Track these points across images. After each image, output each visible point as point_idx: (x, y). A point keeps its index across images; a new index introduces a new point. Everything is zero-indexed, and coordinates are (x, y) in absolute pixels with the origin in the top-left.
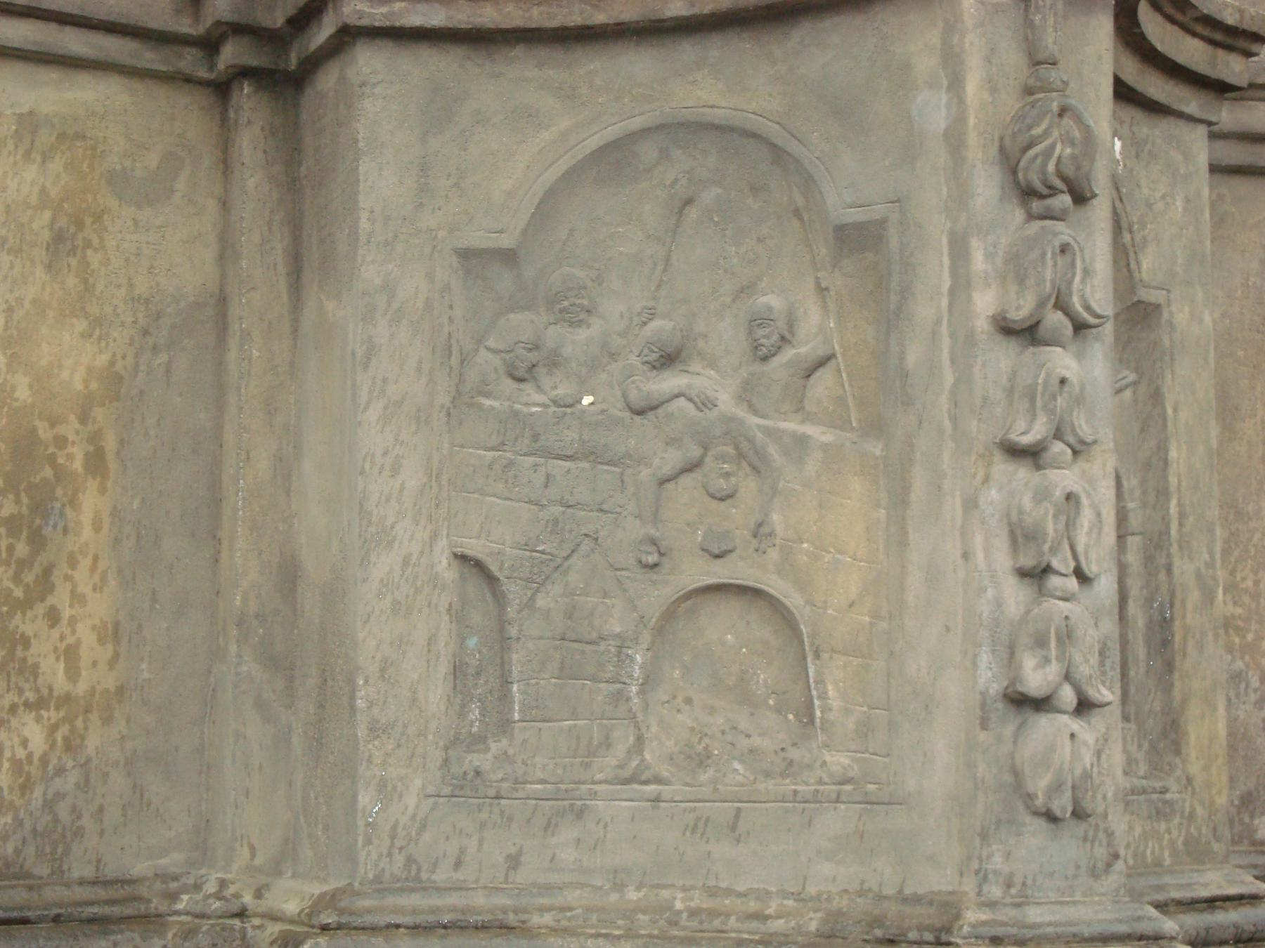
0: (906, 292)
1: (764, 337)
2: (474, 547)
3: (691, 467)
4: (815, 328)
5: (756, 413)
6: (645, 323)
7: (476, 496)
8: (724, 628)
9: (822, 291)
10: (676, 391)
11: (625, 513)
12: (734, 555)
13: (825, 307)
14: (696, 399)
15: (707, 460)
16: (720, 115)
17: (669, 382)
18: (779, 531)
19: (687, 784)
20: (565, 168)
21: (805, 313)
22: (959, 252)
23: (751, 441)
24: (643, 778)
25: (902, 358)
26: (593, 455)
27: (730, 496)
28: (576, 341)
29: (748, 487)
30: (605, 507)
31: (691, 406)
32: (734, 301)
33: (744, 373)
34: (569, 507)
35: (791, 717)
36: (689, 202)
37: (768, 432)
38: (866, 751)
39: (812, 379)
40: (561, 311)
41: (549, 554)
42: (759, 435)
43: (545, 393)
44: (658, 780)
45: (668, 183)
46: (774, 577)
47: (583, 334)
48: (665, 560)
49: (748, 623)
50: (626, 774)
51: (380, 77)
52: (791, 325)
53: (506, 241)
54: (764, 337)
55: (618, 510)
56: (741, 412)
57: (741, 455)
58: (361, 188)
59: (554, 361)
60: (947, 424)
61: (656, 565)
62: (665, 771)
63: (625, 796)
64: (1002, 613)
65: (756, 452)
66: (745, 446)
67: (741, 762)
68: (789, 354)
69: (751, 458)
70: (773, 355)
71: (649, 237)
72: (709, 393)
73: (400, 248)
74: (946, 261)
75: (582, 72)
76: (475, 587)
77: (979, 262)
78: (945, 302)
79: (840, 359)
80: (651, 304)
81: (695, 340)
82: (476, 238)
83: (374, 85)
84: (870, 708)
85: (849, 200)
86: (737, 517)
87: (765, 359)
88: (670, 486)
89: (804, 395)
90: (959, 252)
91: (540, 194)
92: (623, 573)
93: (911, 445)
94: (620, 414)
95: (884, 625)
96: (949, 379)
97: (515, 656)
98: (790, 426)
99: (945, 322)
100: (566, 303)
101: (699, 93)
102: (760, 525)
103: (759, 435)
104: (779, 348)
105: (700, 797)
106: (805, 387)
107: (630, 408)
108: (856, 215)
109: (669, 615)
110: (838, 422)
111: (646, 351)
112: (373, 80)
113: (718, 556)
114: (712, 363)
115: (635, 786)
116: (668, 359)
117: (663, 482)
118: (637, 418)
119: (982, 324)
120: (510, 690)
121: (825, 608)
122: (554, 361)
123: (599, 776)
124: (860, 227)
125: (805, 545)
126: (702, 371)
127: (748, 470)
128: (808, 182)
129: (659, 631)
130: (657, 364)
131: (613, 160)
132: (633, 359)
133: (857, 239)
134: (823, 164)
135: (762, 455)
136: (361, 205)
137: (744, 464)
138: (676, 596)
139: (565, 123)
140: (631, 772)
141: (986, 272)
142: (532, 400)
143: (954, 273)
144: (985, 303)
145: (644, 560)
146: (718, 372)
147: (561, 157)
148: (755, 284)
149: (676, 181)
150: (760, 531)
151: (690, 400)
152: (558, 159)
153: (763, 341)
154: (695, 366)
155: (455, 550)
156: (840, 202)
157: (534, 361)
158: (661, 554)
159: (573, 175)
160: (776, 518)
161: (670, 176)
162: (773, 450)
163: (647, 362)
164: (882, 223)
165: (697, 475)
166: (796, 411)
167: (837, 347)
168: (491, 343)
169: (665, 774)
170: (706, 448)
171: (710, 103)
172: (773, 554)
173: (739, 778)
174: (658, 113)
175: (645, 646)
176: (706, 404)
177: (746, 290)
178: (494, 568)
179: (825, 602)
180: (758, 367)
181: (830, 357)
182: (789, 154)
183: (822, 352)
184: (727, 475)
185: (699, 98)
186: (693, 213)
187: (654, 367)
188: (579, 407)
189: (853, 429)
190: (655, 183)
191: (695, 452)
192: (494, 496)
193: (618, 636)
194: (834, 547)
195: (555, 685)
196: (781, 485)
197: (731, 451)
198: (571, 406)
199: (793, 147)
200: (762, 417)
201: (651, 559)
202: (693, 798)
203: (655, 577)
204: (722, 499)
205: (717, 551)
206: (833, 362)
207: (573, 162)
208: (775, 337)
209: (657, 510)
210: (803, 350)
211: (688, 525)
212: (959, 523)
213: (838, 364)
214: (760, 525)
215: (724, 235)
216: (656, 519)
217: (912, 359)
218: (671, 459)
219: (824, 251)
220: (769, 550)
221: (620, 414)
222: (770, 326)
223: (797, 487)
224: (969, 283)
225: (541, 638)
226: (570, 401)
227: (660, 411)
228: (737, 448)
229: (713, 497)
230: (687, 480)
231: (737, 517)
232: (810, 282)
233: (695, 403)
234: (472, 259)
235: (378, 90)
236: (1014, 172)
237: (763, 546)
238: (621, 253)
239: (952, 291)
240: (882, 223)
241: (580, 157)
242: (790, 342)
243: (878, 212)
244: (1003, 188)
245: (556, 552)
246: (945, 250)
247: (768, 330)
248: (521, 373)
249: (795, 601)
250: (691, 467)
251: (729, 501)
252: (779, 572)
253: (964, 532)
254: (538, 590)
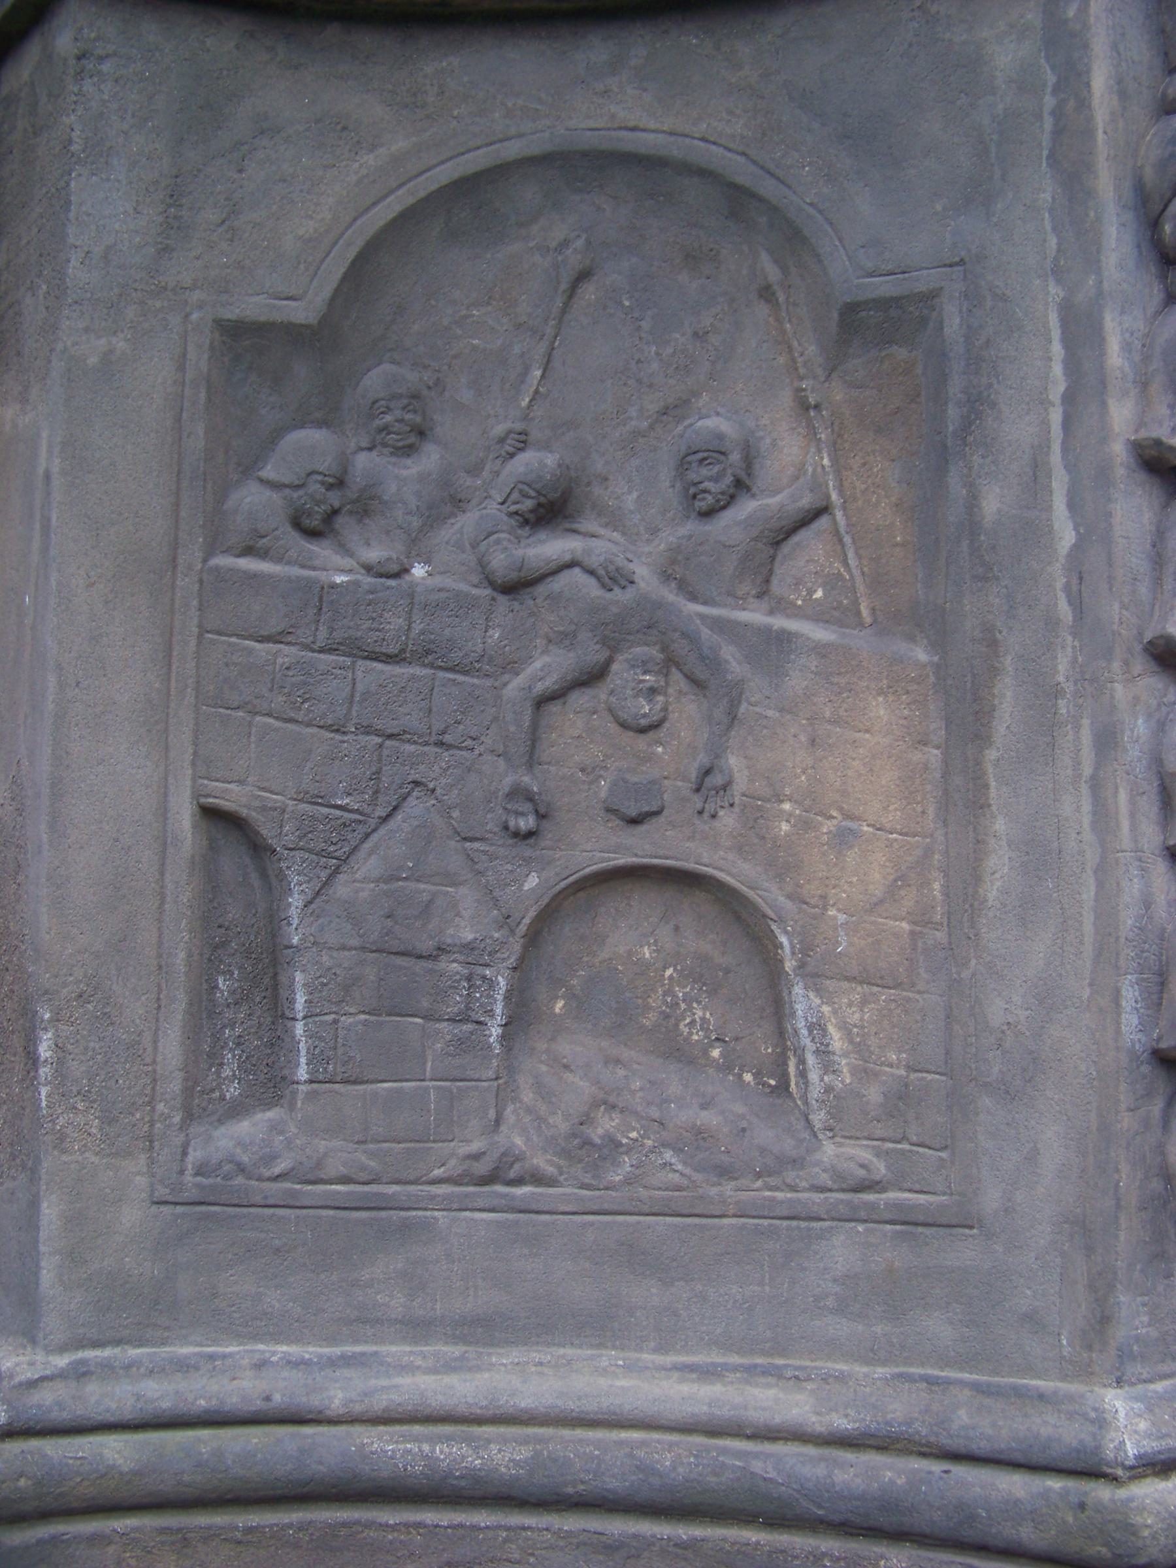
0: (977, 404)
1: (710, 479)
2: (233, 796)
3: (593, 677)
4: (792, 461)
5: (693, 597)
6: (512, 456)
7: (241, 714)
8: (637, 938)
9: (804, 406)
10: (567, 557)
11: (482, 748)
12: (662, 819)
13: (812, 432)
14: (601, 572)
15: (615, 667)
16: (648, 142)
17: (552, 547)
18: (741, 783)
19: (584, 1186)
20: (398, 208)
21: (774, 444)
22: (1081, 331)
23: (691, 638)
24: (512, 1174)
25: (973, 502)
26: (424, 653)
27: (655, 726)
28: (406, 478)
29: (687, 714)
30: (447, 738)
31: (592, 581)
32: (651, 427)
33: (669, 537)
34: (390, 736)
35: (748, 1077)
36: (583, 276)
37: (719, 625)
38: (904, 1139)
39: (786, 548)
40: (380, 430)
41: (357, 811)
42: (705, 632)
43: (352, 556)
44: (538, 1179)
45: (554, 244)
46: (731, 856)
47: (412, 468)
48: (545, 824)
49: (677, 928)
50: (481, 1168)
51: (111, 48)
52: (749, 461)
53: (302, 313)
54: (710, 479)
55: (469, 742)
56: (670, 595)
57: (670, 662)
58: (72, 215)
59: (365, 506)
60: (1064, 609)
61: (530, 834)
62: (543, 1162)
63: (480, 1203)
64: (1150, 918)
65: (702, 658)
66: (681, 647)
67: (678, 1150)
68: (747, 507)
69: (687, 664)
70: (724, 508)
71: (518, 327)
72: (620, 561)
73: (131, 312)
74: (1057, 349)
75: (429, 70)
76: (232, 860)
77: (1115, 357)
78: (1056, 416)
79: (839, 514)
80: (519, 426)
81: (589, 484)
82: (251, 306)
83: (101, 59)
84: (910, 1068)
85: (869, 265)
86: (671, 758)
87: (707, 514)
88: (554, 708)
89: (771, 571)
90: (1081, 331)
91: (360, 243)
92: (476, 845)
93: (993, 644)
94: (474, 591)
95: (941, 936)
96: (1066, 537)
97: (299, 976)
98: (754, 616)
99: (1056, 448)
100: (388, 418)
101: (613, 109)
102: (708, 772)
103: (705, 632)
104: (732, 497)
105: (606, 1206)
106: (773, 558)
107: (492, 584)
108: (884, 287)
109: (550, 914)
110: (839, 614)
111: (515, 495)
112: (99, 52)
113: (635, 821)
114: (615, 520)
115: (500, 1188)
116: (550, 509)
117: (543, 701)
118: (502, 599)
119: (1119, 450)
120: (290, 1032)
121: (825, 908)
122: (365, 506)
123: (438, 1172)
124: (884, 304)
125: (787, 806)
126: (602, 531)
127: (683, 684)
128: (792, 239)
129: (534, 938)
130: (532, 517)
131: (470, 203)
132: (492, 508)
133: (875, 326)
134: (821, 212)
135: (714, 664)
136: (71, 240)
137: (676, 675)
138: (563, 884)
139: (400, 144)
140: (491, 1166)
141: (1121, 369)
142: (335, 568)
143: (1073, 366)
144: (1121, 417)
145: (512, 824)
146: (624, 534)
147: (392, 192)
148: (687, 402)
149: (565, 244)
150: (708, 783)
151: (592, 573)
152: (386, 196)
153: (707, 485)
154: (589, 524)
155: (202, 800)
156: (848, 270)
157: (337, 504)
158: (541, 816)
159: (409, 219)
160: (733, 761)
161: (559, 233)
162: (729, 653)
163: (516, 513)
164: (930, 298)
165: (601, 693)
166: (760, 596)
167: (834, 496)
168: (269, 472)
169: (551, 1170)
170: (614, 649)
171: (631, 124)
172: (728, 820)
173: (675, 1178)
174: (547, 135)
175: (512, 962)
176: (614, 578)
177: (675, 410)
178: (267, 831)
179: (823, 897)
180: (692, 526)
181: (822, 510)
182: (761, 200)
183: (806, 501)
184: (653, 691)
185: (613, 117)
186: (589, 292)
187: (526, 522)
188: (407, 577)
189: (861, 625)
190: (531, 244)
191: (594, 654)
192: (269, 715)
193: (469, 947)
194: (840, 809)
195: (365, 1023)
196: (743, 708)
197: (655, 652)
198: (396, 575)
199: (768, 188)
200: (705, 603)
201: (526, 823)
202: (595, 1208)
203: (528, 853)
204: (642, 731)
205: (633, 812)
206: (823, 522)
207: (411, 201)
208: (728, 479)
209: (533, 747)
210: (774, 501)
211: (583, 770)
212: (1087, 771)
213: (835, 523)
214: (708, 772)
215: (639, 328)
216: (531, 761)
217: (992, 504)
218: (546, 666)
219: (812, 349)
220: (721, 813)
221: (474, 591)
222: (719, 462)
223: (770, 713)
224: (1103, 383)
225: (343, 948)
226: (395, 568)
227: (541, 589)
228: (664, 649)
229: (624, 725)
230: (580, 699)
231: (671, 758)
232: (786, 398)
233: (598, 578)
234: (246, 344)
235: (106, 67)
236: (1155, 224)
237: (710, 807)
238: (475, 348)
239: (1069, 398)
240: (930, 298)
241: (422, 194)
242: (748, 489)
243: (924, 281)
244: (1139, 246)
245: (368, 810)
246: (1056, 334)
247: (716, 469)
248: (315, 522)
249: (769, 895)
250: (593, 677)
251: (651, 735)
252: (739, 849)
253: (1096, 785)
254: (337, 871)
